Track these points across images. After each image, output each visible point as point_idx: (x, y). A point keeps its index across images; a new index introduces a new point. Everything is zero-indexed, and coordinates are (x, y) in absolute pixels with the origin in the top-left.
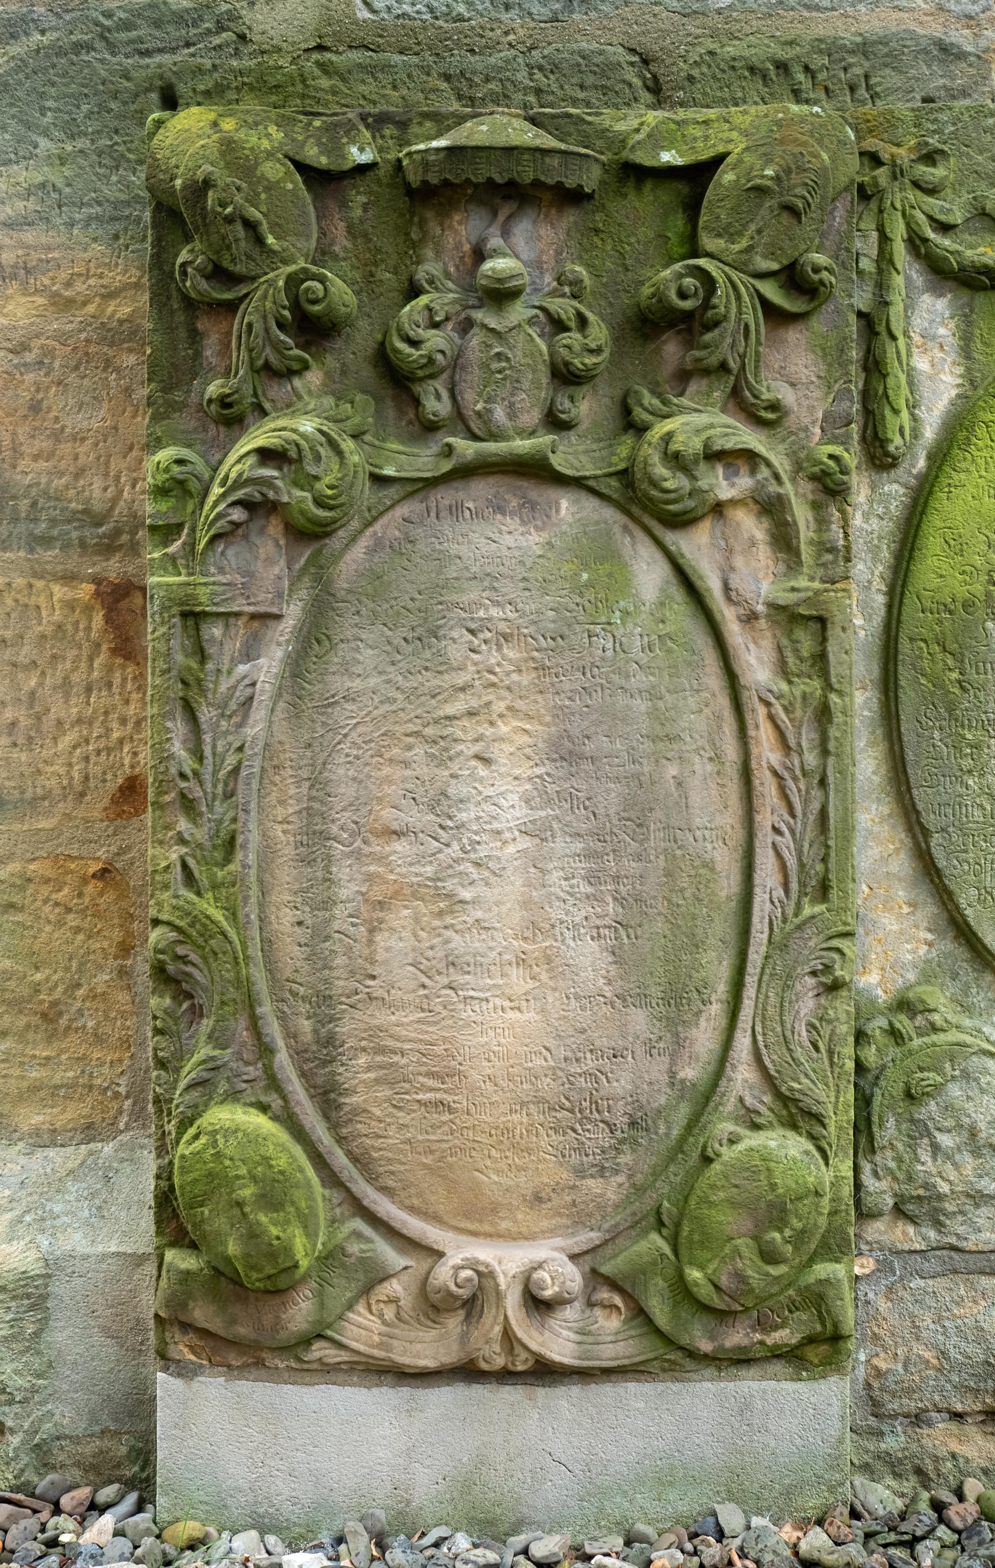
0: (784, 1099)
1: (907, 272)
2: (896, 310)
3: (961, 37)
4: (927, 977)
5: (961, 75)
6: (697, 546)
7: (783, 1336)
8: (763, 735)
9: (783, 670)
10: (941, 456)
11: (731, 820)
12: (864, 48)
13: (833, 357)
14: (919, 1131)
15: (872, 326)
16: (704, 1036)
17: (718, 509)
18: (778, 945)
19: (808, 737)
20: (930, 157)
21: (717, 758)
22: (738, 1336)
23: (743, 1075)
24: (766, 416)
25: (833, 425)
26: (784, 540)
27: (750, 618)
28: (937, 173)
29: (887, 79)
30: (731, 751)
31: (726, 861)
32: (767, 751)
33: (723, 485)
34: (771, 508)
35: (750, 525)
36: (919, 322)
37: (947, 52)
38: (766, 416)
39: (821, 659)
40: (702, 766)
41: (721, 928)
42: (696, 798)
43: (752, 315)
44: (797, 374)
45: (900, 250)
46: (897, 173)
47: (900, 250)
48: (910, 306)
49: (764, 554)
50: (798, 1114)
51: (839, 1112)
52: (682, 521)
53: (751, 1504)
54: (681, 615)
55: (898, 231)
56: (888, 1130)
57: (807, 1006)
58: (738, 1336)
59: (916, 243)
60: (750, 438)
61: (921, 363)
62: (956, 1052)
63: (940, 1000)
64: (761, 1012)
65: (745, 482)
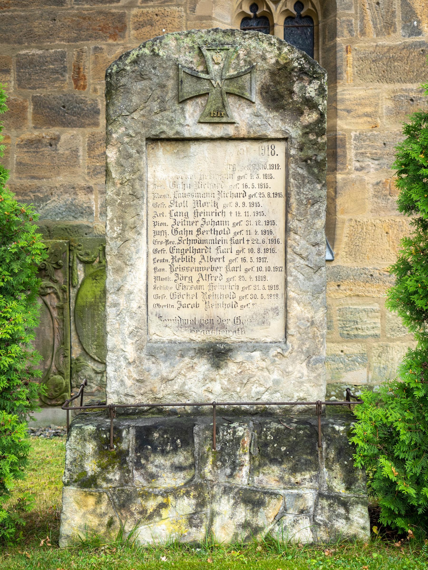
0: (59, 371)
1: (76, 261)
2: (75, 266)
3: (90, 225)
4: (80, 356)
5: (90, 230)
6: (47, 298)
7: (59, 402)
8: (56, 323)
9: (58, 315)
10: (81, 285)
11: (51, 334)
12: (77, 226)
13: (65, 274)
14: (78, 376)
15: (71, 268)
16: (48, 363)
17: (49, 294)
18: (58, 351)
19: (61, 324)
20: (80, 245)
21: (50, 326)
22: (53, 402)
23: (54, 368)
24: (56, 282)
25: (65, 282)
26: (58, 297)
27: (54, 308)
28: (80, 248)
29: (80, 231)
30: (52, 325)
31: (51, 339)
32: (56, 325)
33: (49, 291)
34: (56, 293)
35: (54, 296)
36: (78, 268)
37: (88, 227)
38: (56, 282)
39: (63, 313)
40: (47, 327)
41: (50, 348)
42: (46, 331)
43: (52, 269)
44: (59, 276)
45: (75, 258)
46: (75, 248)
47: (75, 258)
48: (77, 265)
49: (56, 300)
50: (61, 373)
51: (67, 372)
52: (44, 295)
53: (55, 424)
54: (45, 308)
55: (75, 255)
56: (74, 376)
57: (62, 359)
58: (53, 402)
59: (77, 257)
60: (52, 284)
61: (79, 273)
62: (83, 366)
63: (82, 359)
64: (56, 360)
65: (52, 290)
